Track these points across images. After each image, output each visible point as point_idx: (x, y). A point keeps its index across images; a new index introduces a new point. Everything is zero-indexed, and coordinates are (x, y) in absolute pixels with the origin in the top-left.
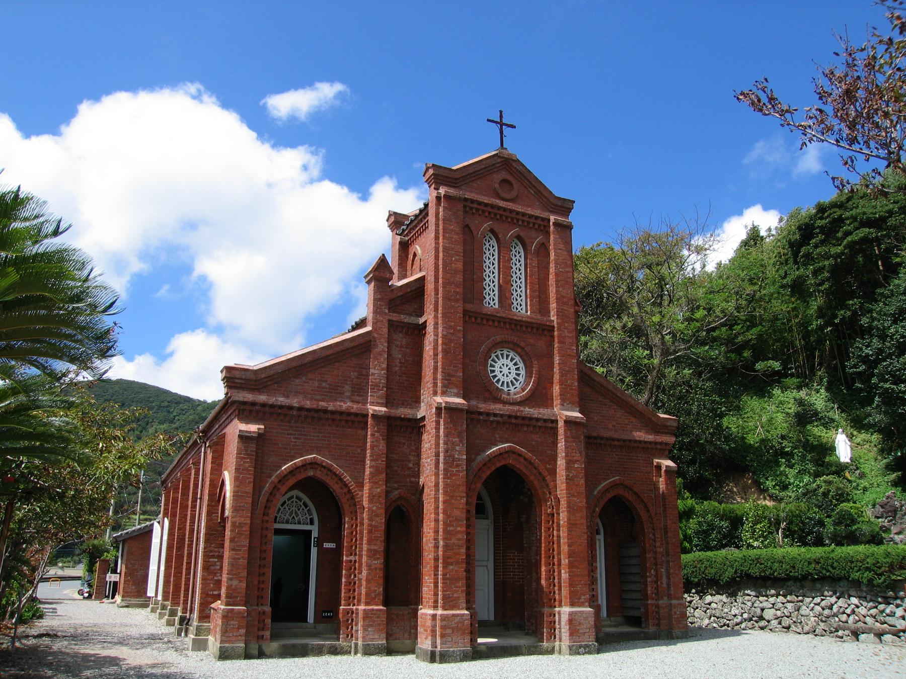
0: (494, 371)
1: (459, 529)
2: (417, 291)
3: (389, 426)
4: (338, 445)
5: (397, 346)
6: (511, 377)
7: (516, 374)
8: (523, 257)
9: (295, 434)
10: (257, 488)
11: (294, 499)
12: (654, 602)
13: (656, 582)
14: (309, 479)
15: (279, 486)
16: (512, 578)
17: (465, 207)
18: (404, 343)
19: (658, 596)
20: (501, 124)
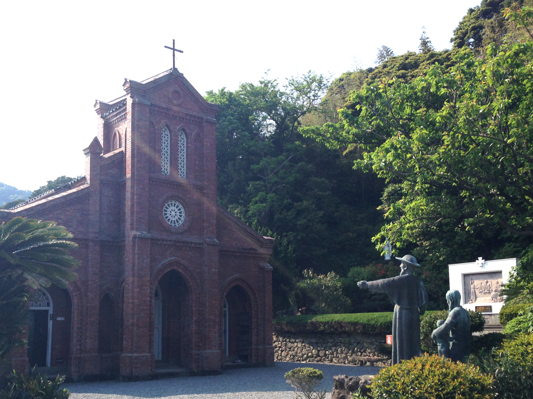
17: (150, 109)
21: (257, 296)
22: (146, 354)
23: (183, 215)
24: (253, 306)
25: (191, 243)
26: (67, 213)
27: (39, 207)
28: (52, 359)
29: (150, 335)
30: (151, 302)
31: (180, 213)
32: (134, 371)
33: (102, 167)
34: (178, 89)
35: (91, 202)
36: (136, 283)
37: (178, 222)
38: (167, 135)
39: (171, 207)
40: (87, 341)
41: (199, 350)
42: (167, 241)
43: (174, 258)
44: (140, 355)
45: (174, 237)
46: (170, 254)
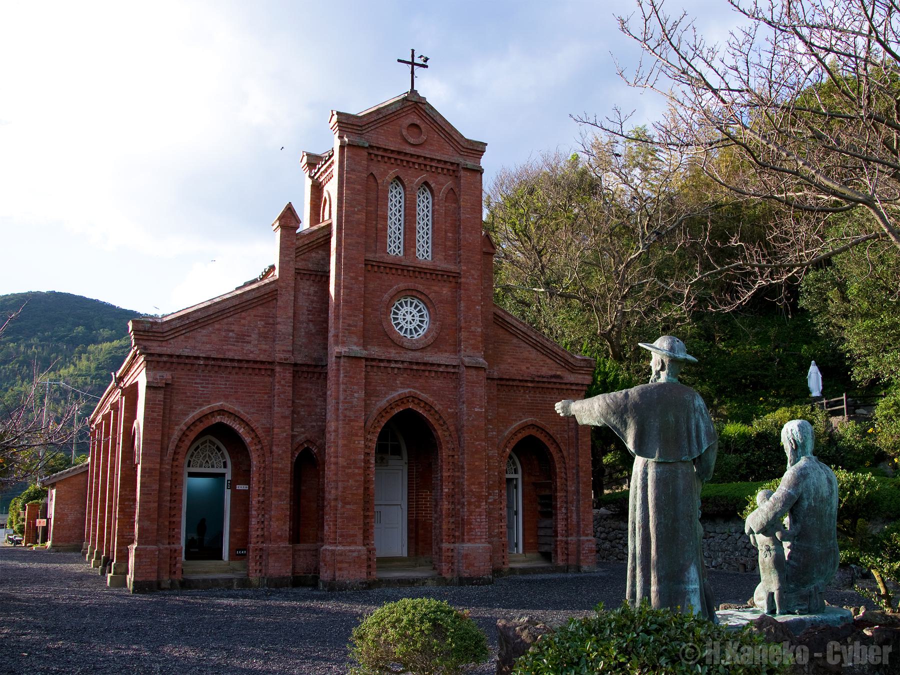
0: (397, 319)
1: (356, 471)
2: (321, 239)
3: (295, 374)
4: (245, 392)
5: (304, 294)
6: (414, 324)
7: (420, 321)
8: (431, 203)
9: (203, 383)
10: (165, 434)
11: (208, 444)
12: (564, 539)
13: (567, 519)
14: (220, 425)
15: (188, 433)
16: (424, 516)
17: (370, 154)
18: (312, 292)
19: (568, 533)
20: (413, 64)
21: (565, 453)
22: (360, 548)
23: (426, 319)
24: (558, 470)
25: (439, 365)
26: (243, 321)
27: (199, 313)
28: (230, 549)
29: (366, 517)
30: (367, 462)
31: (421, 316)
32: (337, 574)
33: (298, 248)
34: (418, 122)
35: (280, 303)
36: (340, 430)
37: (416, 331)
38: (400, 193)
39: (405, 308)
40: (272, 523)
41: (453, 543)
42: (396, 362)
43: (409, 390)
44: (348, 548)
45: (409, 356)
46: (401, 383)
